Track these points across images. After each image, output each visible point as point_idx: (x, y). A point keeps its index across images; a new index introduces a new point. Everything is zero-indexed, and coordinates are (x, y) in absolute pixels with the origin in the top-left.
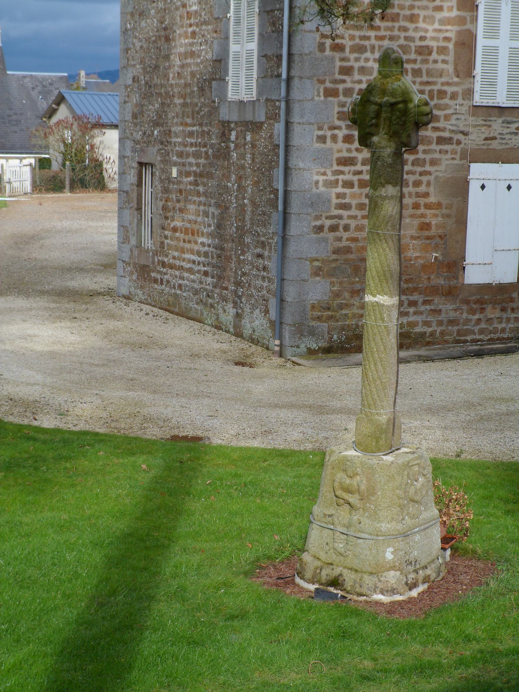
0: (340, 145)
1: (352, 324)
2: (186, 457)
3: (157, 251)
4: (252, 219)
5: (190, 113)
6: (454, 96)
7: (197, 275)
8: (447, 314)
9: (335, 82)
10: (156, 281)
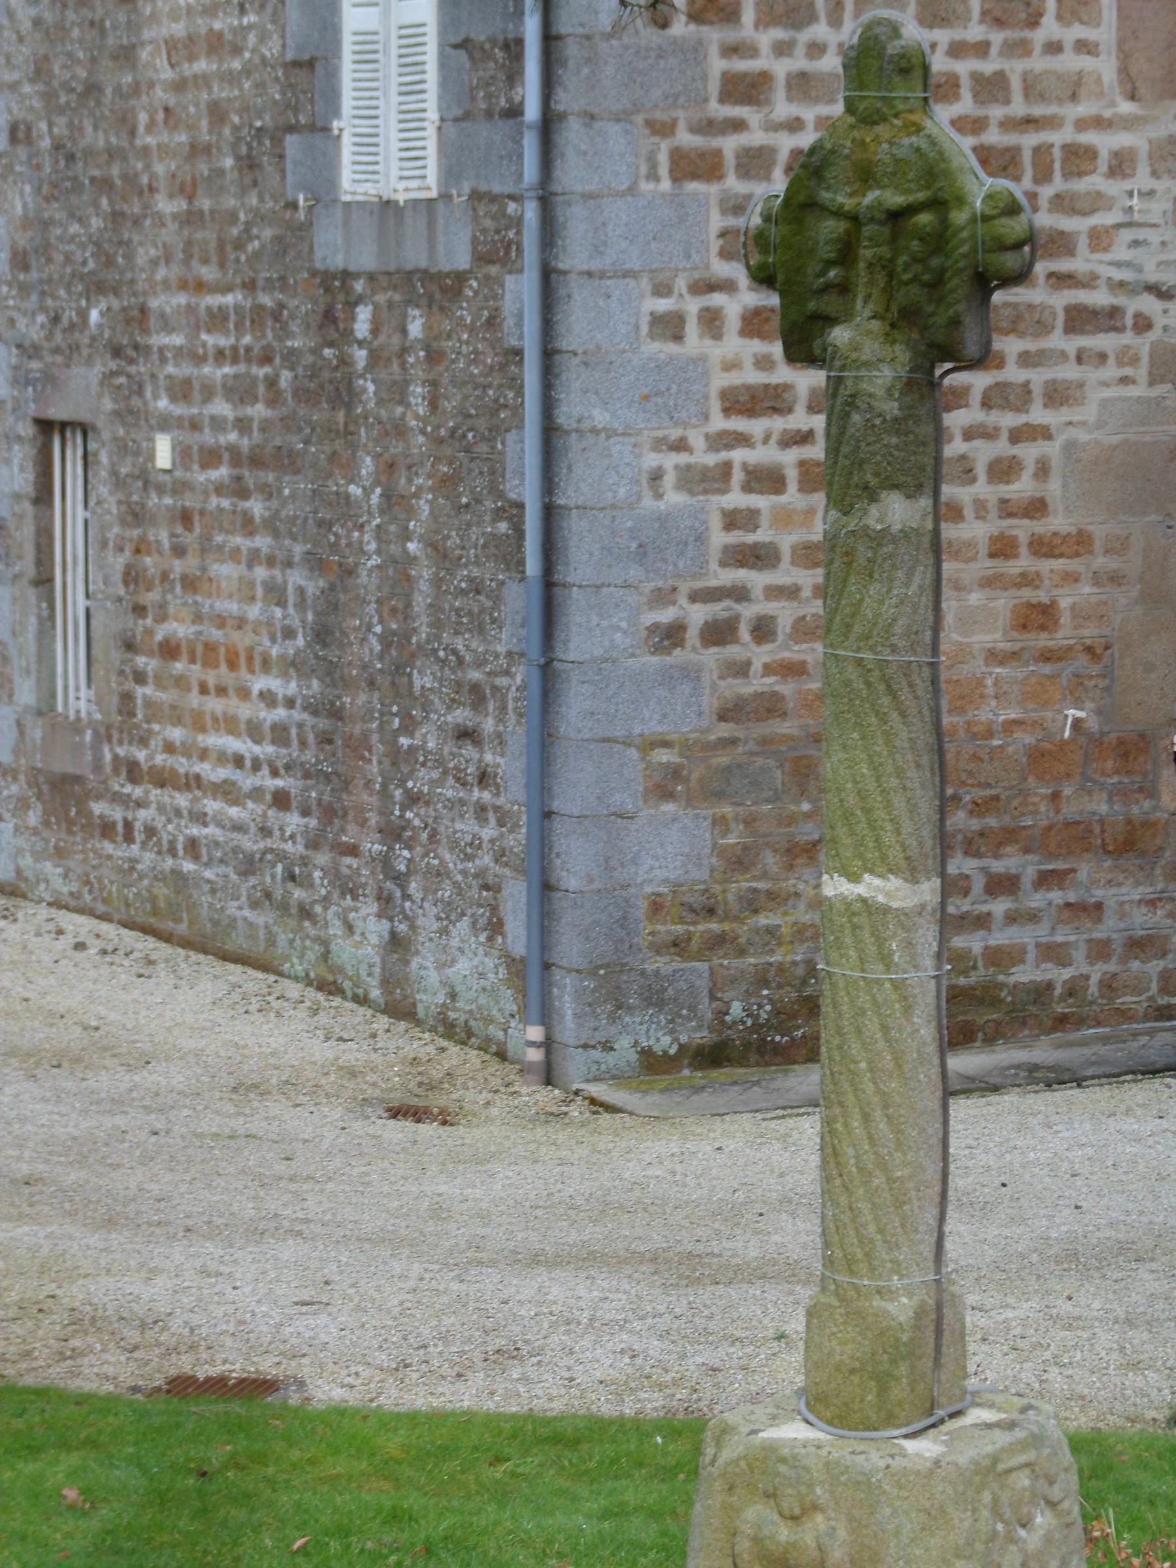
0: (733, 344)
1: (795, 963)
2: (218, 1454)
3: (109, 727)
4: (434, 608)
5: (213, 245)
6: (1121, 165)
7: (250, 805)
8: (1122, 916)
9: (709, 127)
10: (107, 829)
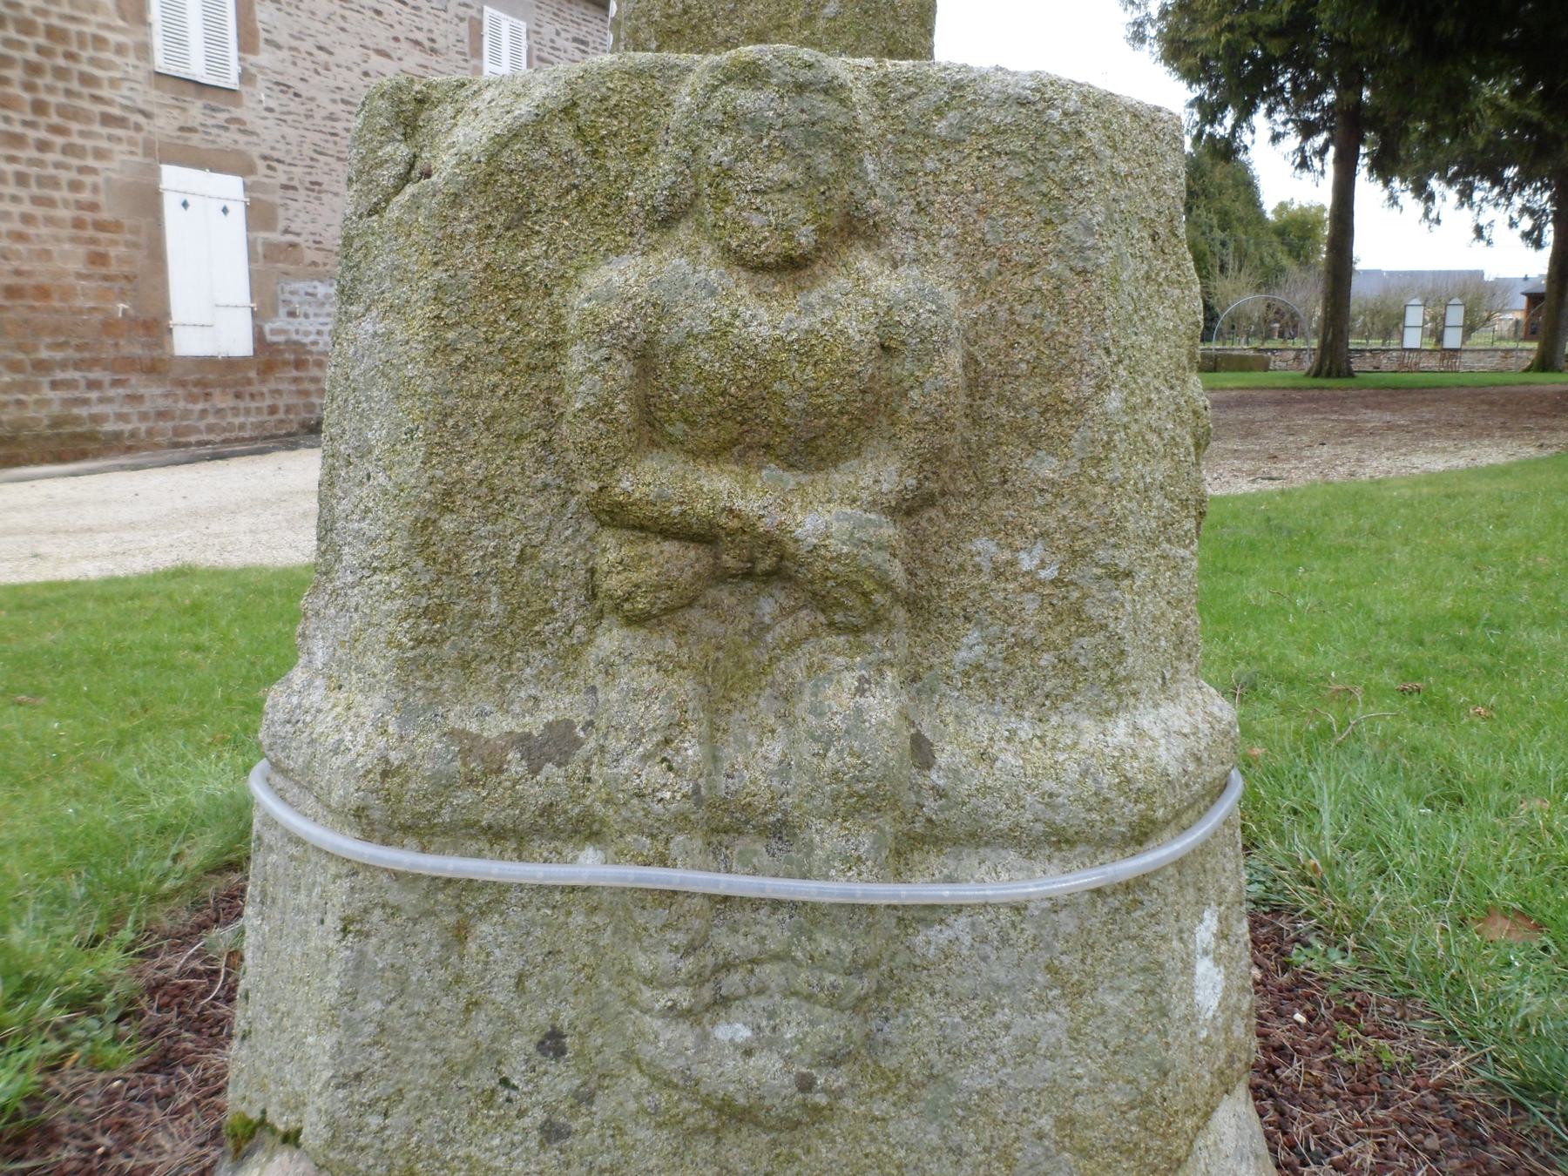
6: (120, 50)
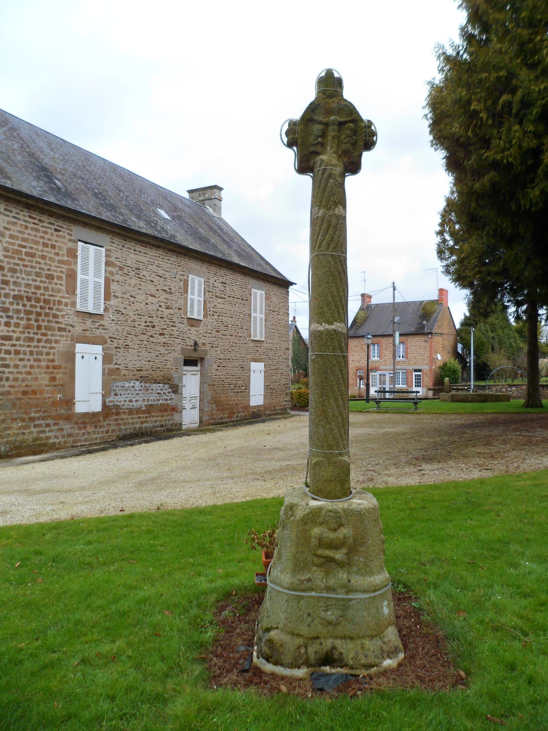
6: (66, 304)
